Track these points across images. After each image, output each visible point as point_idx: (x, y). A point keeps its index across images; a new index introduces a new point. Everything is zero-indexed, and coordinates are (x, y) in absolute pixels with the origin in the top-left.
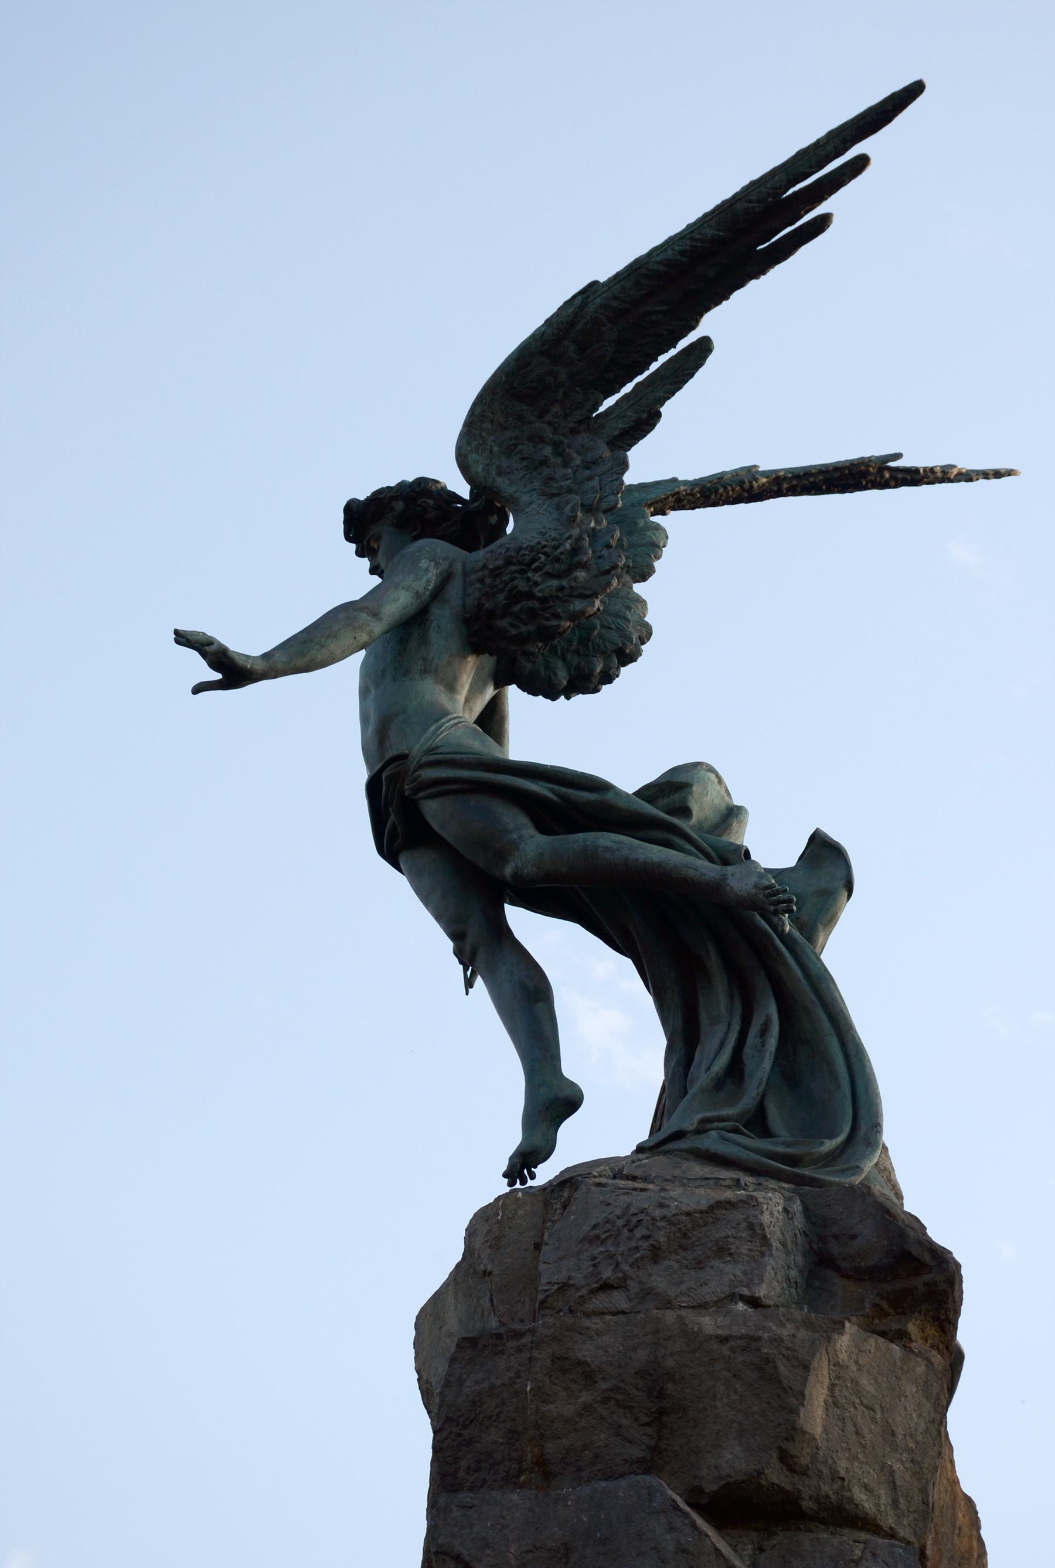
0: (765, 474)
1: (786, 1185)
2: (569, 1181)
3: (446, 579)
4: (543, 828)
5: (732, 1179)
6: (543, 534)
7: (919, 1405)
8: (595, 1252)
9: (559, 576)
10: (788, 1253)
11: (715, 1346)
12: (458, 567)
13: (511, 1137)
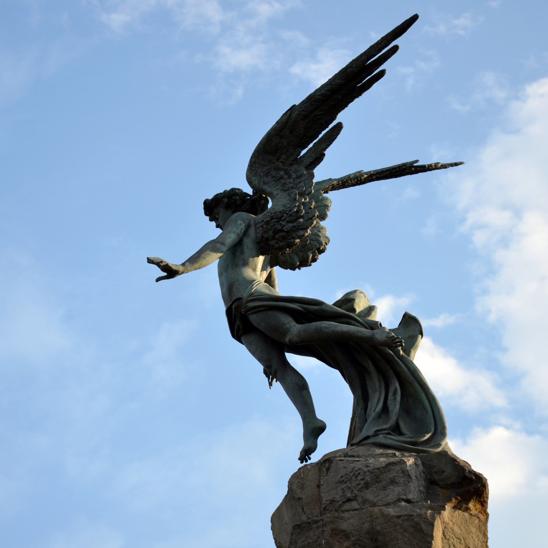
0: (366, 173)
1: (413, 454)
2: (328, 460)
3: (248, 227)
4: (299, 322)
5: (393, 453)
6: (285, 206)
7: (478, 536)
8: (343, 487)
9: (292, 222)
10: (418, 481)
11: (395, 520)
12: (252, 222)
13: (300, 444)
